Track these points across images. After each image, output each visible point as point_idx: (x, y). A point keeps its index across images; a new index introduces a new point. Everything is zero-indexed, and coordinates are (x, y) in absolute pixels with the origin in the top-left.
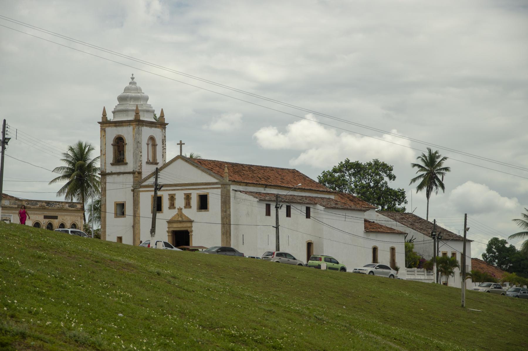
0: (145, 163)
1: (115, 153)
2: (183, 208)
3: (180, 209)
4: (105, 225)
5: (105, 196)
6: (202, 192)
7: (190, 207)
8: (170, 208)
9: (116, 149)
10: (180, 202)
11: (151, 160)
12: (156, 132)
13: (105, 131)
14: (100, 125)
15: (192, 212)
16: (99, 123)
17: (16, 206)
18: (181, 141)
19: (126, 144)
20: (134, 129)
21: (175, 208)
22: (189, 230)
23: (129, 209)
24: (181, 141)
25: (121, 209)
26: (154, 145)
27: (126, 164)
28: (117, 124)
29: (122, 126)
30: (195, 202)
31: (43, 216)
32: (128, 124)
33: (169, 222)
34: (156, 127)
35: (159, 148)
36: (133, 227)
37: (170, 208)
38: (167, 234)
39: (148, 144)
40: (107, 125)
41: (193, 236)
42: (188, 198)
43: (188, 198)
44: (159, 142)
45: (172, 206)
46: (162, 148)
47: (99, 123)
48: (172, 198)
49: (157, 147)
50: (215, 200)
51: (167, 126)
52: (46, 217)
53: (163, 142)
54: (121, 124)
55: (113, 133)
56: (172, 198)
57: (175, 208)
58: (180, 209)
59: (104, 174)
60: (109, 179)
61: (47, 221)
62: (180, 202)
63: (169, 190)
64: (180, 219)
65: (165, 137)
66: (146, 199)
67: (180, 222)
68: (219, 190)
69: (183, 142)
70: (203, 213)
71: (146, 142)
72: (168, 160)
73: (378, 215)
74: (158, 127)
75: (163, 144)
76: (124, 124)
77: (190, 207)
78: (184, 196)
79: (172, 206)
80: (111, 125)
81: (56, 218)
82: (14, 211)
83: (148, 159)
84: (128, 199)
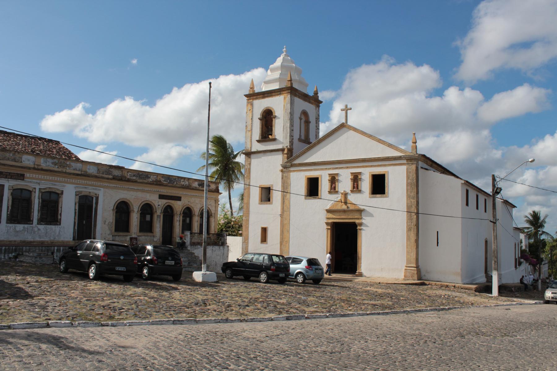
0: (297, 140)
1: (262, 128)
2: (350, 192)
3: (345, 195)
4: (249, 211)
5: (249, 179)
6: (378, 170)
7: (360, 191)
8: (330, 192)
9: (264, 124)
10: (345, 184)
11: (303, 138)
12: (310, 108)
13: (252, 105)
14: (246, 98)
15: (363, 199)
16: (246, 96)
17: (110, 177)
18: (346, 106)
19: (260, 119)
20: (285, 98)
21: (337, 192)
22: (357, 221)
23: (276, 196)
24: (346, 106)
25: (266, 194)
26: (307, 122)
27: (274, 140)
28: (266, 95)
29: (271, 96)
30: (366, 184)
31: (158, 196)
32: (278, 93)
33: (328, 211)
34: (310, 102)
35: (312, 126)
36: (281, 216)
37: (330, 192)
38: (325, 226)
39: (301, 119)
40: (254, 97)
41: (363, 232)
42: (356, 179)
43: (356, 179)
44: (312, 119)
45: (333, 189)
46: (315, 128)
47: (246, 96)
48: (333, 180)
49: (311, 125)
50: (397, 178)
51: (320, 105)
52: (162, 197)
53: (316, 121)
54: (270, 95)
55: (261, 105)
56: (333, 180)
57: (337, 192)
58: (345, 195)
59: (248, 154)
60: (255, 161)
61: (164, 202)
62: (345, 184)
63: (330, 169)
64: (344, 207)
65: (319, 116)
66: (299, 180)
67: (344, 211)
68: (404, 168)
69: (344, 108)
70: (378, 200)
71: (299, 115)
72: (321, 134)
73: (40, 237)
74: (312, 104)
75: (317, 123)
76: (274, 94)
77: (360, 191)
78: (350, 177)
79: (333, 189)
80: (258, 97)
81: (179, 199)
82: (106, 184)
83: (300, 136)
84: (274, 180)
